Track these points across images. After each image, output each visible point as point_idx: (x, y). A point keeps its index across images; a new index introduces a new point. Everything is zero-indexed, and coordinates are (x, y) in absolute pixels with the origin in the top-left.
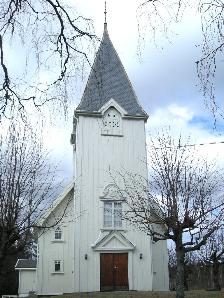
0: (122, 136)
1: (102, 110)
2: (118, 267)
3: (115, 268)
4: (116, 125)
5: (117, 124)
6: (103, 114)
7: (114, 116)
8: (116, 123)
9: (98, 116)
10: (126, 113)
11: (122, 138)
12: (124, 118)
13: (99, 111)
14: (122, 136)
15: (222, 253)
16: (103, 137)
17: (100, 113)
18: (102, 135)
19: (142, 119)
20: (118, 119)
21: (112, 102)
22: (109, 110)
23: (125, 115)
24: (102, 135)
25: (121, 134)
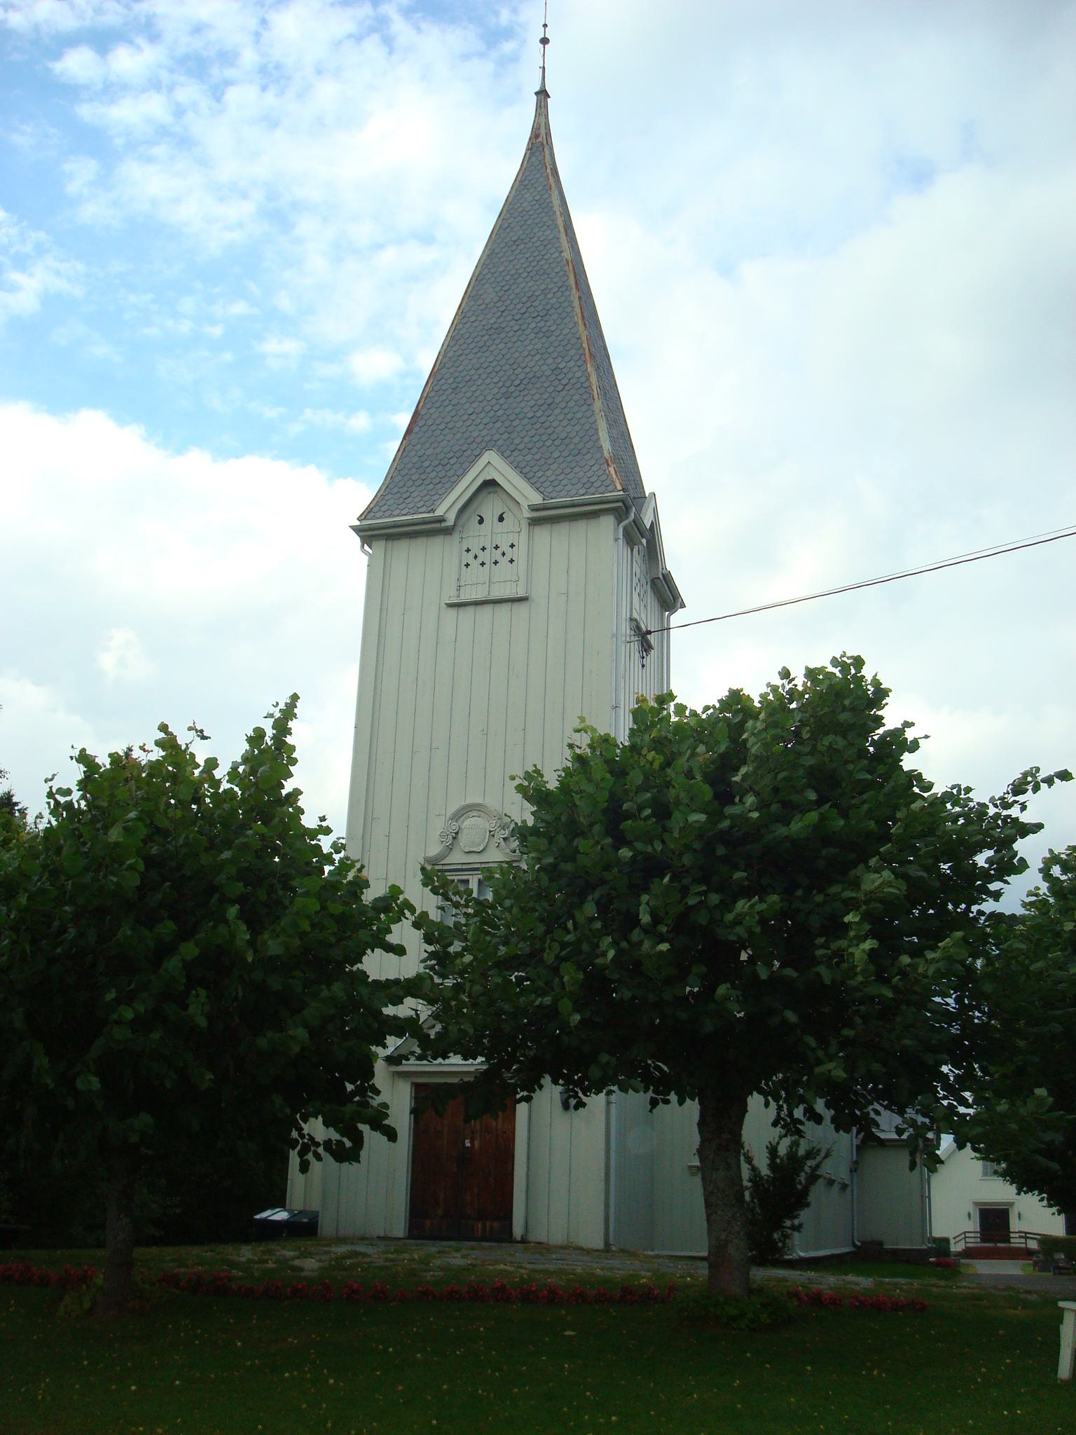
0: (523, 599)
1: (447, 508)
2: (477, 1144)
3: (468, 1144)
4: (501, 555)
5: (508, 557)
6: (450, 521)
7: (501, 519)
8: (504, 547)
9: (436, 529)
10: (537, 499)
11: (521, 609)
12: (534, 522)
13: (439, 512)
14: (523, 599)
15: (73, 7)
16: (453, 612)
17: (441, 520)
18: (450, 605)
19: (606, 511)
20: (512, 532)
21: (492, 464)
22: (485, 492)
23: (534, 508)
24: (450, 605)
25: (521, 593)
